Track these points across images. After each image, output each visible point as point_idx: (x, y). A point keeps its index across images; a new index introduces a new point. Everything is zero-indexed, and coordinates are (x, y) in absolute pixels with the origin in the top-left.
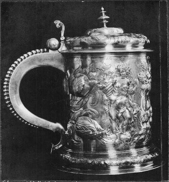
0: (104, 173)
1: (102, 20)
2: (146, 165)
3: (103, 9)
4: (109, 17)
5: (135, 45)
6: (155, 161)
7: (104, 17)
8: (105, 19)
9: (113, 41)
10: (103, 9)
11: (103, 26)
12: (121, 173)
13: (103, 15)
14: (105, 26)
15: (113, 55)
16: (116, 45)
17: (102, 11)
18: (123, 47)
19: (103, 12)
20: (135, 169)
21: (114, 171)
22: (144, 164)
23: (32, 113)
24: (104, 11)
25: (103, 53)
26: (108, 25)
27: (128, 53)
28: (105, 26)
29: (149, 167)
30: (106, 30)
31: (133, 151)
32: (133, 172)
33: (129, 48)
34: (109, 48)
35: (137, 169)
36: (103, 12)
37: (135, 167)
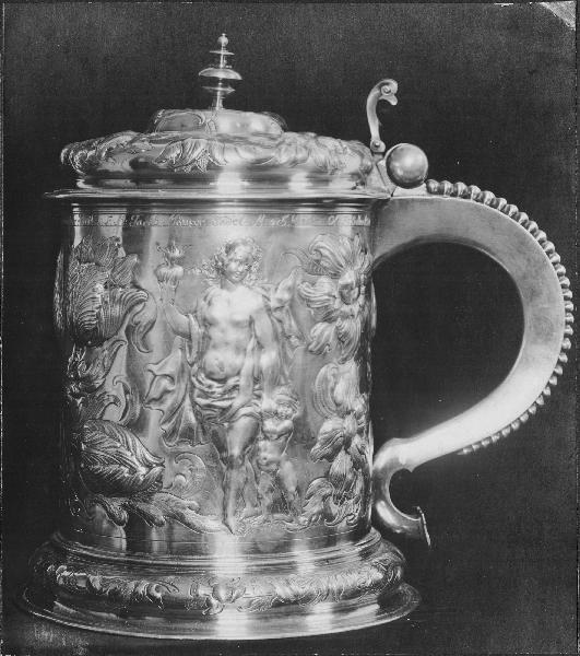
0: (199, 631)
1: (215, 81)
2: (352, 609)
3: (224, 40)
4: (239, 78)
5: (320, 175)
6: (387, 598)
7: (224, 73)
8: (226, 82)
9: (245, 156)
10: (224, 40)
11: (206, 103)
12: (259, 634)
13: (221, 66)
14: (219, 103)
15: (242, 209)
16: (260, 173)
17: (219, 47)
18: (282, 180)
19: (223, 52)
20: (219, 625)
21: (231, 625)
22: (346, 601)
23: (513, 363)
24: (228, 47)
25: (212, 203)
26: (230, 103)
27: (338, 201)
28: (219, 103)
29: (366, 616)
30: (224, 120)
31: (303, 556)
32: (305, 634)
33: (299, 186)
34: (229, 185)
35: (320, 621)
36: (223, 52)
37: (335, 612)
